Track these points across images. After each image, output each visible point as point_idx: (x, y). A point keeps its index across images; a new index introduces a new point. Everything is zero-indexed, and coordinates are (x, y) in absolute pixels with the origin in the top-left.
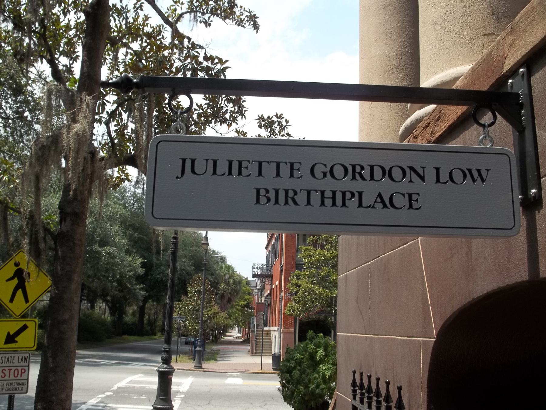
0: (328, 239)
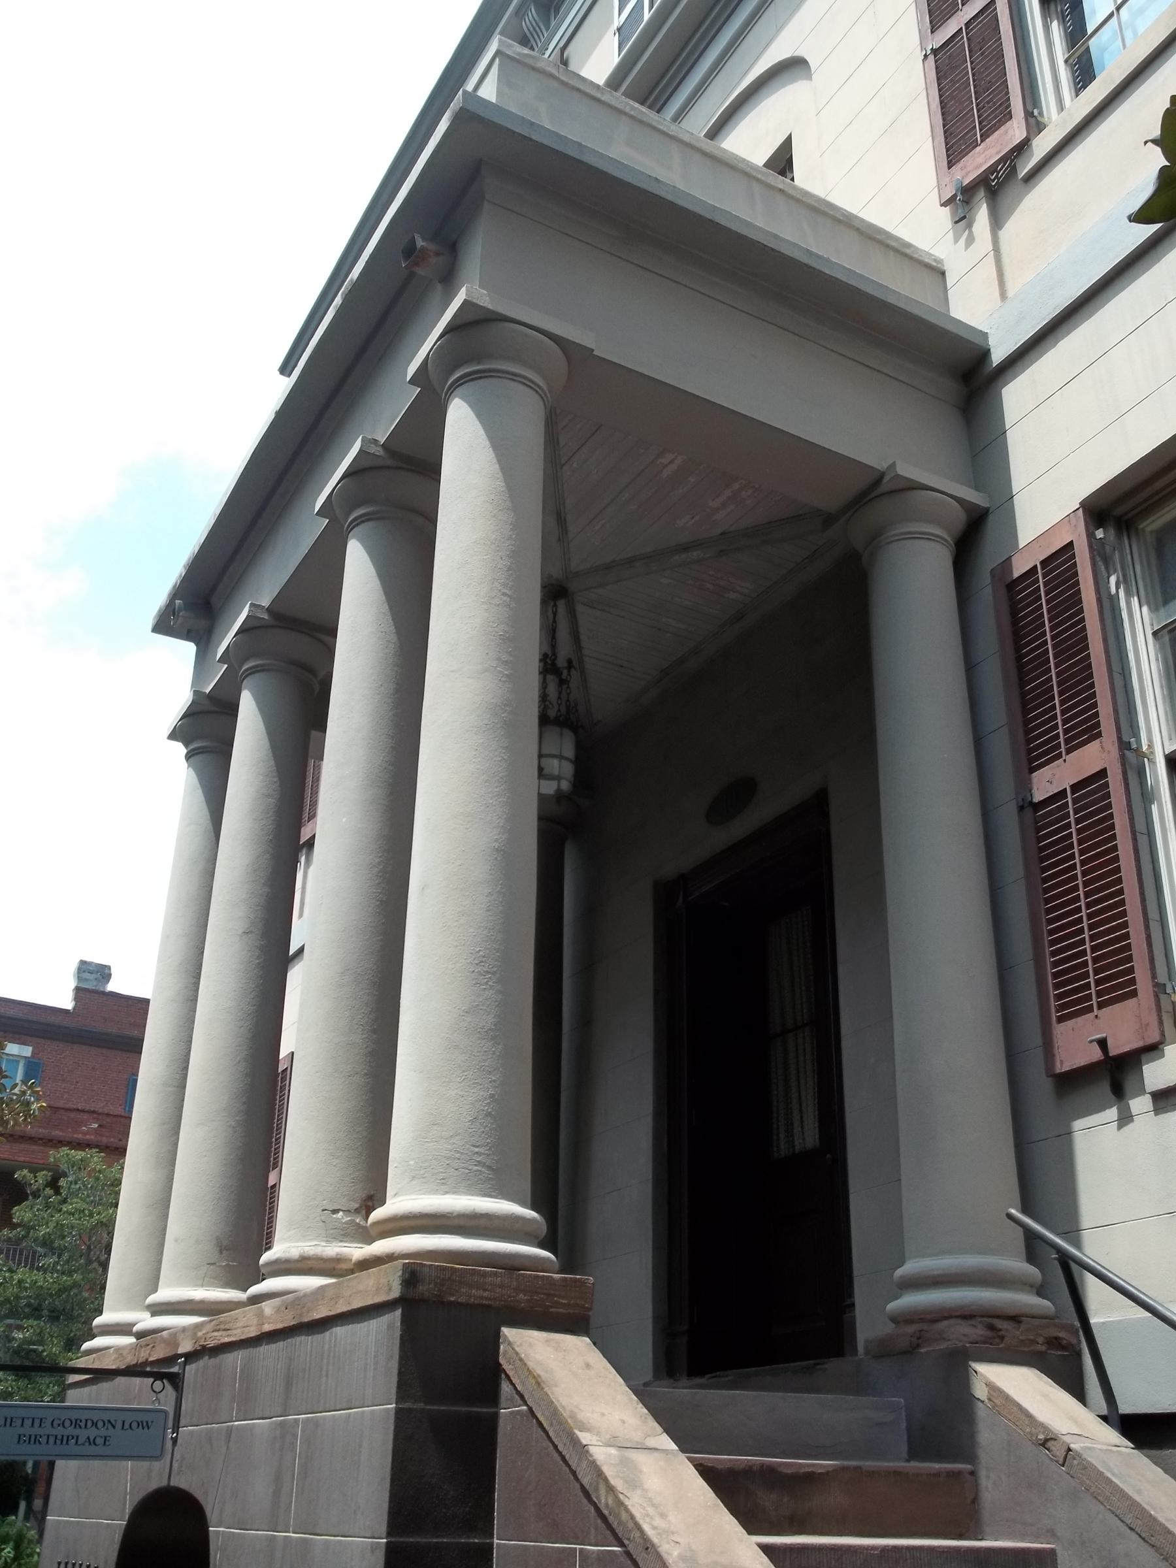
0: (52, 1242)
